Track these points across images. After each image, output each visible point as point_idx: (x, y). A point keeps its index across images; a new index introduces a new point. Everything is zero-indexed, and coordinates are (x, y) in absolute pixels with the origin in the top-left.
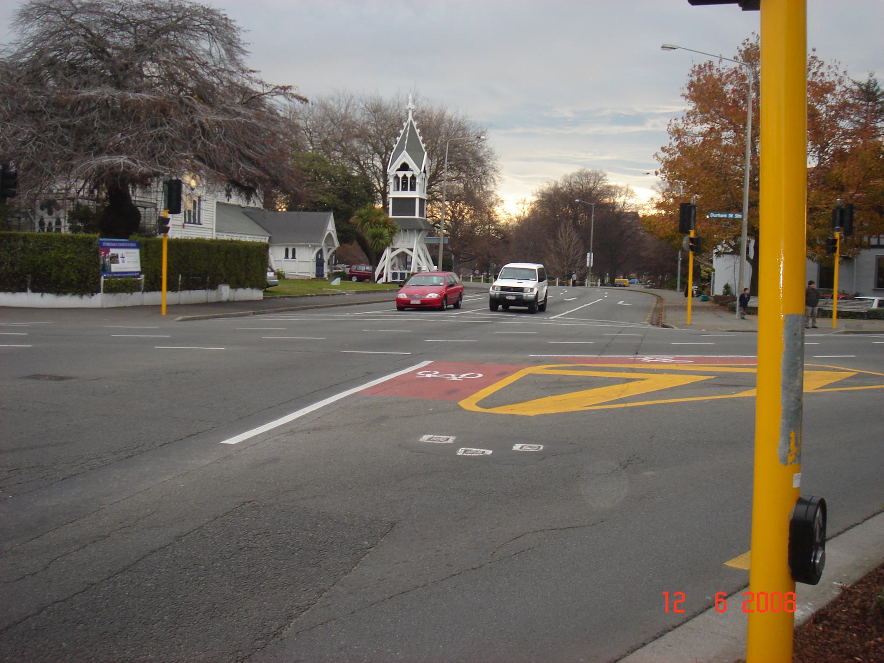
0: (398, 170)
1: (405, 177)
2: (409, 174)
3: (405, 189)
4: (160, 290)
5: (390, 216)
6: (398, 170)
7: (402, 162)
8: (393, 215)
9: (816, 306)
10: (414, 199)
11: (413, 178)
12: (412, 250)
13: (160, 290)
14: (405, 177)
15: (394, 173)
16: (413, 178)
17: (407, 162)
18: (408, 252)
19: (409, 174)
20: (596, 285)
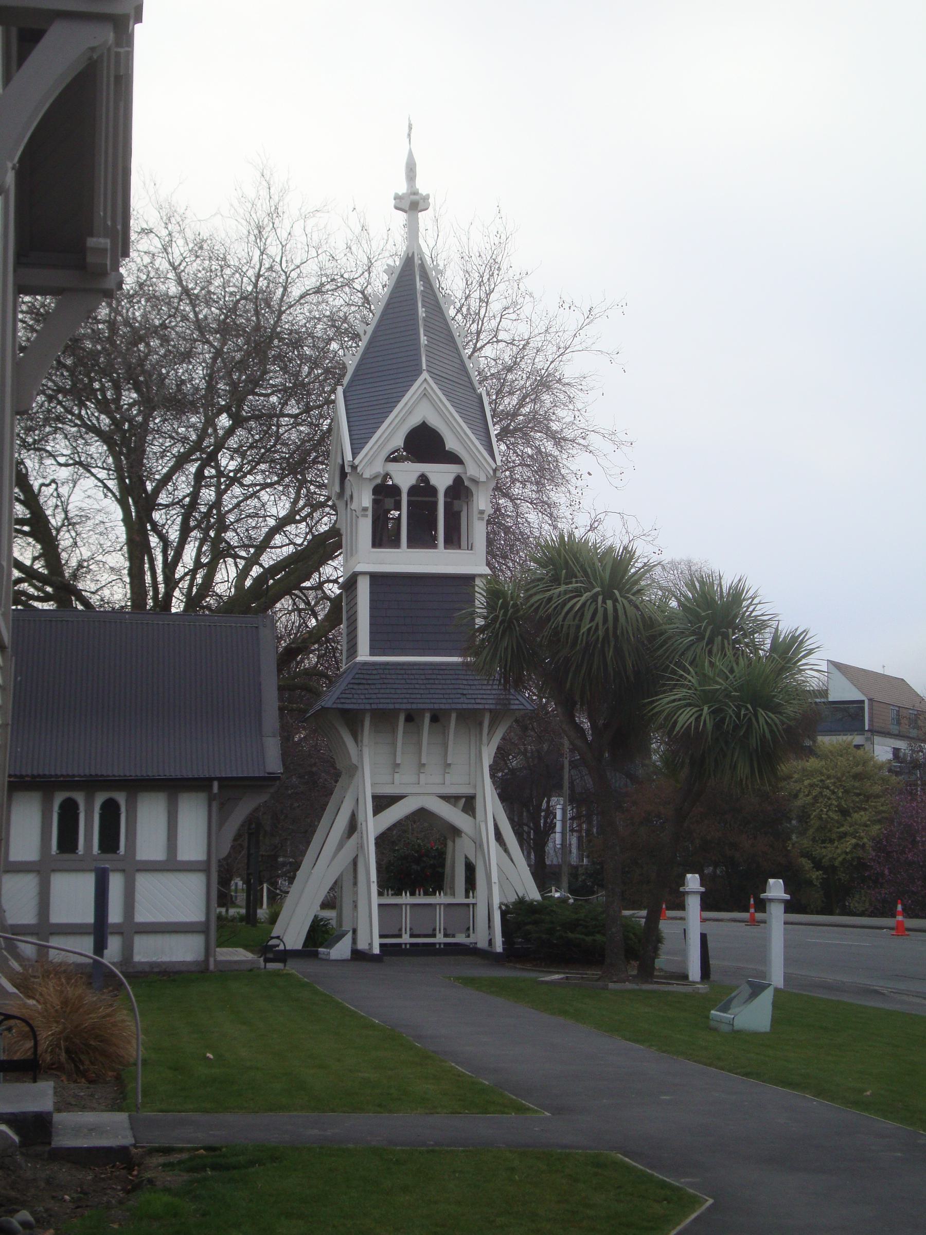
0: (392, 458)
1: (423, 488)
2: (441, 476)
3: (422, 535)
4: (435, 546)
5: (364, 655)
6: (392, 458)
7: (414, 421)
8: (373, 651)
9: (905, 917)
10: (469, 579)
11: (459, 491)
12: (469, 804)
13: (435, 546)
14: (423, 488)
15: (378, 467)
16: (459, 491)
17: (435, 422)
18: (452, 815)
19: (441, 476)
20: (474, 905)
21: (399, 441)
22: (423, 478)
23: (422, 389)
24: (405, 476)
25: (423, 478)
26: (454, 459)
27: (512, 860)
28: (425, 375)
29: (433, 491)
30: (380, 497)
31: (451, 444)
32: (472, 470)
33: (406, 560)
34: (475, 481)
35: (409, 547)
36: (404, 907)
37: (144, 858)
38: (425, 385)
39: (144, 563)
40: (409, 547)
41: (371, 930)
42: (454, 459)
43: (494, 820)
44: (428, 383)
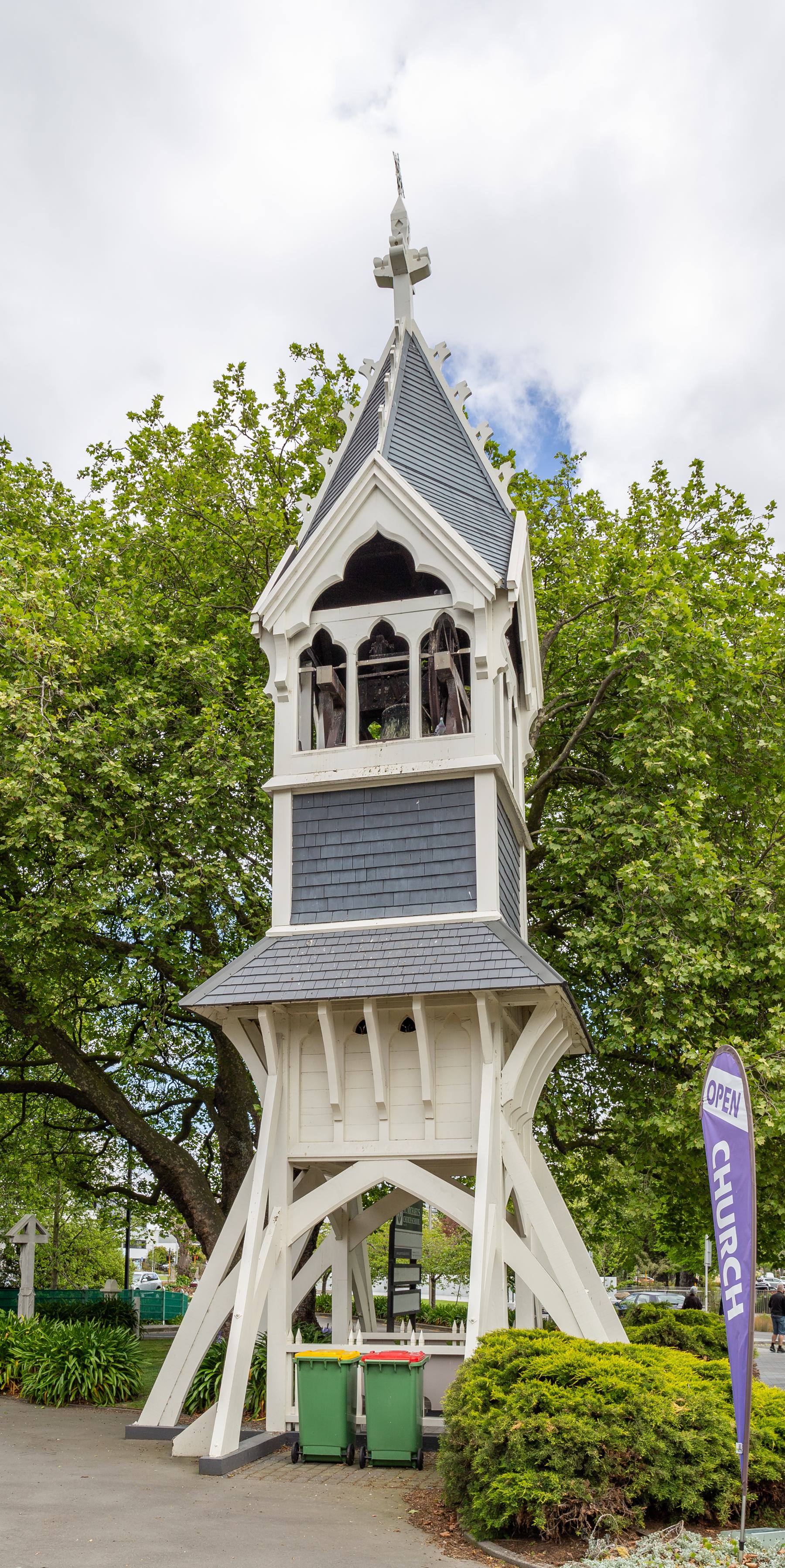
0: (330, 599)
1: (384, 637)
3: (381, 712)
6: (330, 599)
7: (359, 534)
8: (296, 915)
10: (461, 784)
11: (449, 635)
14: (384, 637)
17: (396, 529)
19: (412, 618)
21: (334, 571)
22: (383, 630)
23: (371, 475)
25: (383, 630)
26: (432, 585)
29: (401, 646)
31: (424, 560)
32: (463, 595)
34: (469, 615)
37: (297, 1414)
38: (375, 470)
39: (248, 1121)
42: (432, 585)
44: (380, 468)
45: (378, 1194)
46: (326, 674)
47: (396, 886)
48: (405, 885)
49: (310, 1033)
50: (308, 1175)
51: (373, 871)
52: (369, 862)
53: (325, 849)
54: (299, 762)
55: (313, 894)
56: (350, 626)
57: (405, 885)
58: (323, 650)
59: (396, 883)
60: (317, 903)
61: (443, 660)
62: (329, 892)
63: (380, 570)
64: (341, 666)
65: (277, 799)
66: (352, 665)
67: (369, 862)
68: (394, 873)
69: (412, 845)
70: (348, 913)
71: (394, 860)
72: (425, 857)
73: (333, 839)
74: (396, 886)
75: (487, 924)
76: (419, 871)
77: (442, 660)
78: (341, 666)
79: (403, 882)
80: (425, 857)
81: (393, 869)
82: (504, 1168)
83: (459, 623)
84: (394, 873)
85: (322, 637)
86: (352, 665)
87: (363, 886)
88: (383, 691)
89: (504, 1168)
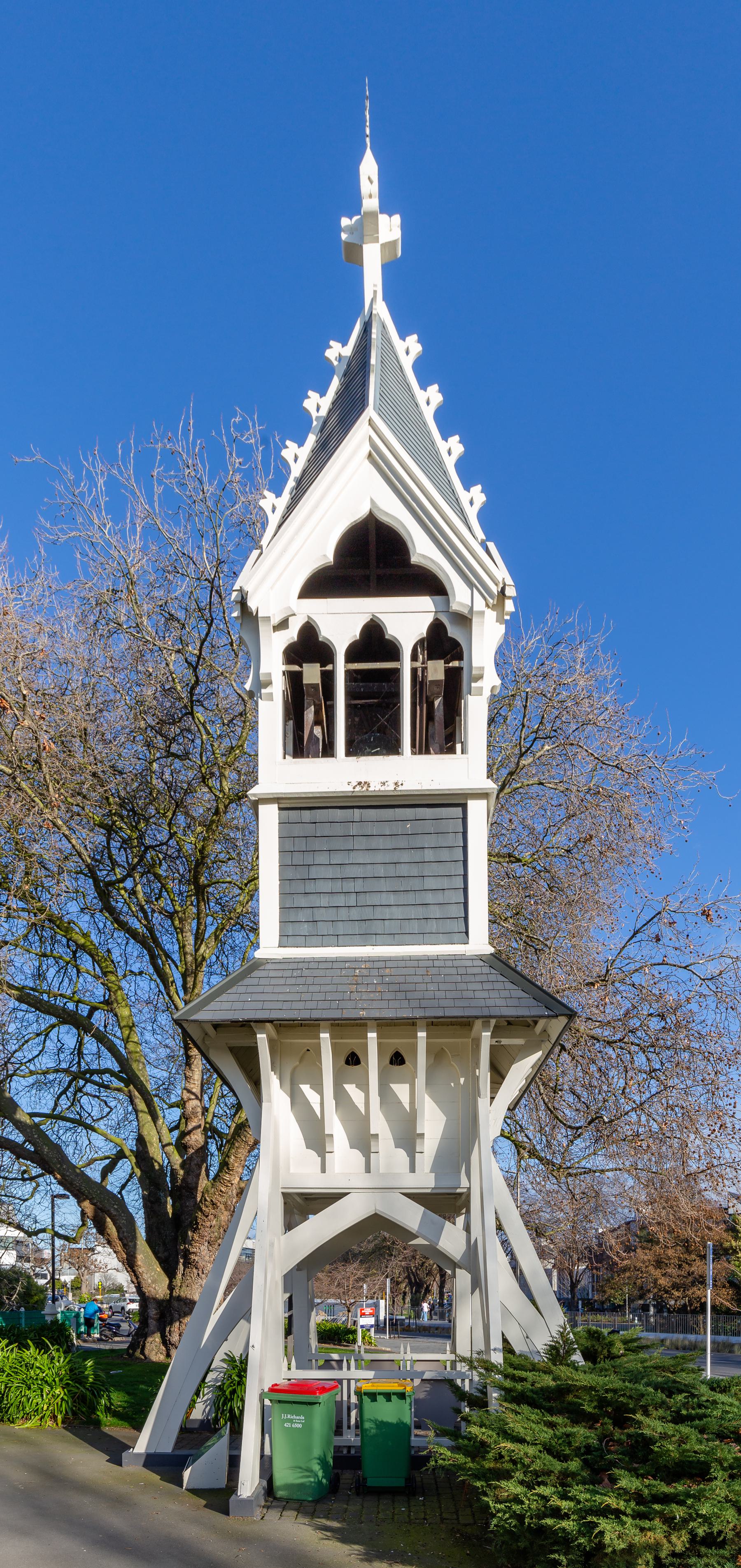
0: (320, 585)
1: (374, 642)
3: (374, 732)
6: (320, 585)
8: (285, 939)
10: (457, 802)
11: (441, 643)
14: (374, 642)
19: (407, 619)
21: (324, 552)
24: (342, 621)
26: (428, 583)
27: (280, 526)
28: (370, 412)
29: (392, 651)
30: (296, 668)
31: (423, 550)
33: (339, 773)
35: (348, 753)
36: (345, 1383)
40: (348, 753)
41: (294, 1402)
42: (428, 583)
43: (497, 1219)
45: (376, 1223)
46: (312, 674)
47: (387, 913)
48: (397, 913)
49: (301, 1060)
50: (301, 1206)
51: (362, 895)
52: (359, 886)
53: (313, 869)
54: (279, 773)
55: (302, 916)
56: (342, 621)
57: (397, 913)
58: (309, 647)
59: (387, 910)
60: (306, 925)
61: (436, 670)
62: (320, 915)
63: (371, 559)
64: (329, 667)
65: (262, 808)
66: (340, 668)
67: (359, 886)
68: (385, 899)
69: (404, 870)
70: (337, 940)
71: (383, 885)
72: (416, 884)
73: (322, 858)
74: (387, 913)
75: (481, 958)
76: (410, 898)
77: (436, 670)
78: (329, 667)
79: (394, 909)
80: (416, 884)
81: (384, 895)
82: (636, 933)
83: (452, 631)
84: (385, 899)
85: (309, 631)
86: (340, 668)
87: (353, 910)
88: (375, 698)
89: (636, 933)
